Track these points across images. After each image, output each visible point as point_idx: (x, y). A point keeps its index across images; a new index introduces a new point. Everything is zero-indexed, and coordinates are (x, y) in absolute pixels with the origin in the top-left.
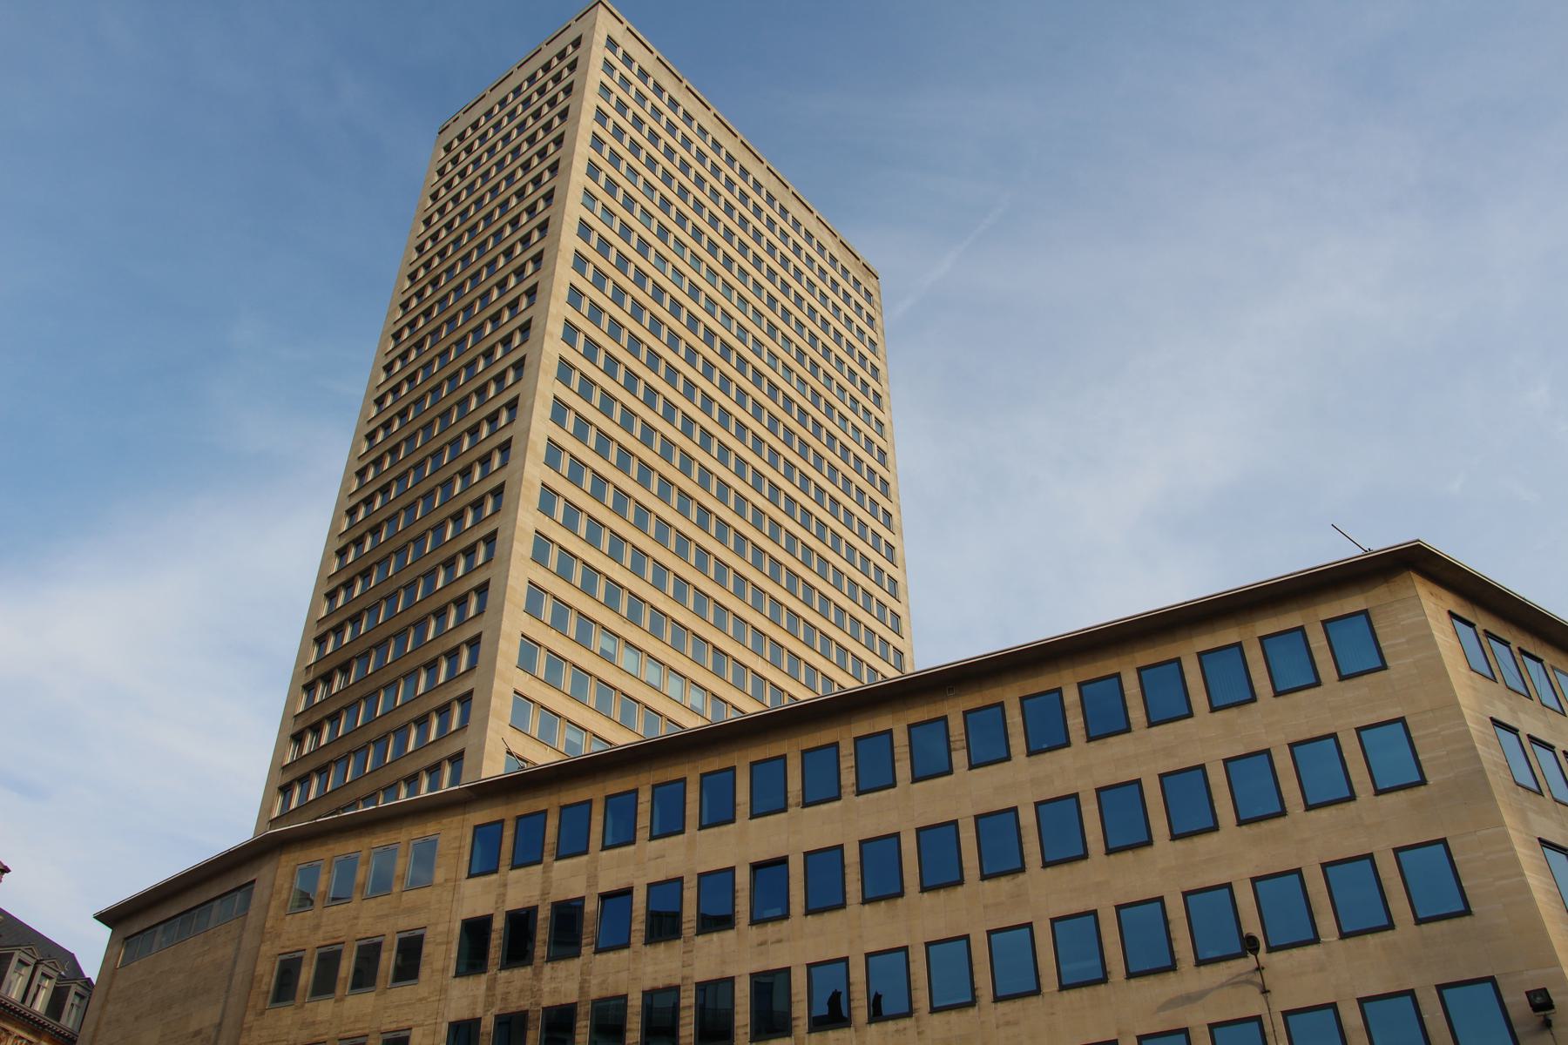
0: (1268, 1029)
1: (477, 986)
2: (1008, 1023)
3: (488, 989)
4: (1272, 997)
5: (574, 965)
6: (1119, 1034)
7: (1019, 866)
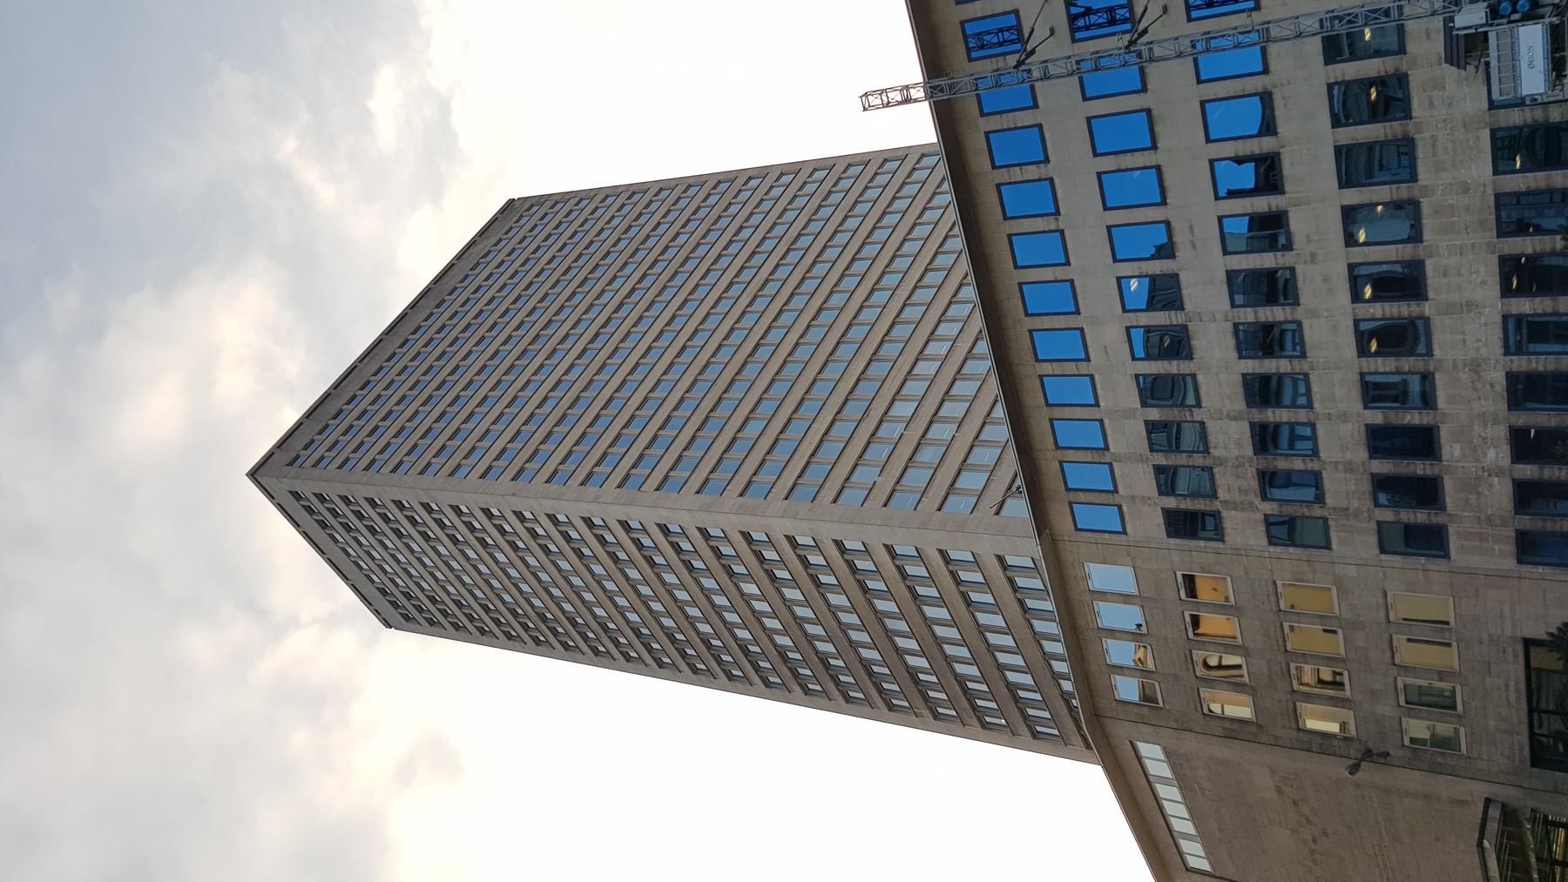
1: (1231, 519)
3: (1235, 509)
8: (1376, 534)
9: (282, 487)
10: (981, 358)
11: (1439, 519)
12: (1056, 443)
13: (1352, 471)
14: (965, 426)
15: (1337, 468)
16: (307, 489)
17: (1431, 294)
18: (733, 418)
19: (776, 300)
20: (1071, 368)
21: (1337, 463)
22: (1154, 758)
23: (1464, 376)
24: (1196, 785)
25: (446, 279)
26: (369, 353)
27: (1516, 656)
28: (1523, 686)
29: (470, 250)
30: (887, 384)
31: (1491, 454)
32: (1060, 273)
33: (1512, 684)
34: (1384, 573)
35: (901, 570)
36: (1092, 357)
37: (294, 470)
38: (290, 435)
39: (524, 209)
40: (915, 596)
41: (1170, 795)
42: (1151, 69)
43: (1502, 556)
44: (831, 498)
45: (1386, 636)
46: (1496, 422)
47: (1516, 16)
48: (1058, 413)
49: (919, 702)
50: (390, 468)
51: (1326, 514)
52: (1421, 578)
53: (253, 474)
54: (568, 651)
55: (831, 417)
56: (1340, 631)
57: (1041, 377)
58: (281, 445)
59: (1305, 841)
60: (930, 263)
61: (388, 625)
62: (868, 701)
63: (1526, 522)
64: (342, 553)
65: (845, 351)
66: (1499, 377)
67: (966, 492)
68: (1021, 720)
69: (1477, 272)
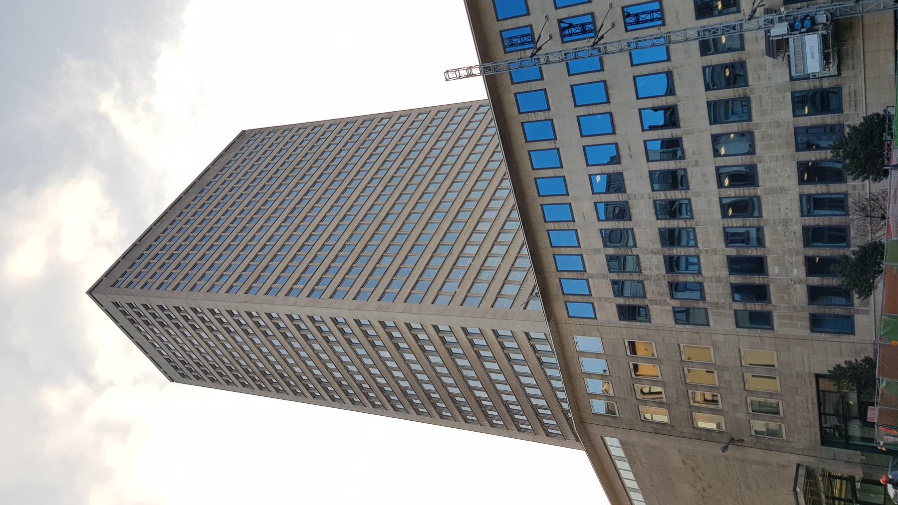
1: (654, 310)
2: (677, 17)
3: (656, 304)
8: (733, 317)
9: (108, 300)
12: (557, 268)
14: (506, 259)
16: (123, 300)
17: (761, 183)
21: (711, 277)
23: (780, 228)
25: (205, 176)
31: (795, 272)
33: (809, 399)
37: (114, 289)
39: (251, 136)
43: (802, 328)
46: (797, 254)
49: (482, 417)
51: (706, 306)
53: (90, 292)
54: (279, 393)
56: (715, 372)
57: (548, 231)
60: (485, 167)
61: (172, 380)
62: (453, 417)
63: (815, 309)
65: (438, 217)
66: (798, 229)
68: (540, 426)
69: (785, 171)
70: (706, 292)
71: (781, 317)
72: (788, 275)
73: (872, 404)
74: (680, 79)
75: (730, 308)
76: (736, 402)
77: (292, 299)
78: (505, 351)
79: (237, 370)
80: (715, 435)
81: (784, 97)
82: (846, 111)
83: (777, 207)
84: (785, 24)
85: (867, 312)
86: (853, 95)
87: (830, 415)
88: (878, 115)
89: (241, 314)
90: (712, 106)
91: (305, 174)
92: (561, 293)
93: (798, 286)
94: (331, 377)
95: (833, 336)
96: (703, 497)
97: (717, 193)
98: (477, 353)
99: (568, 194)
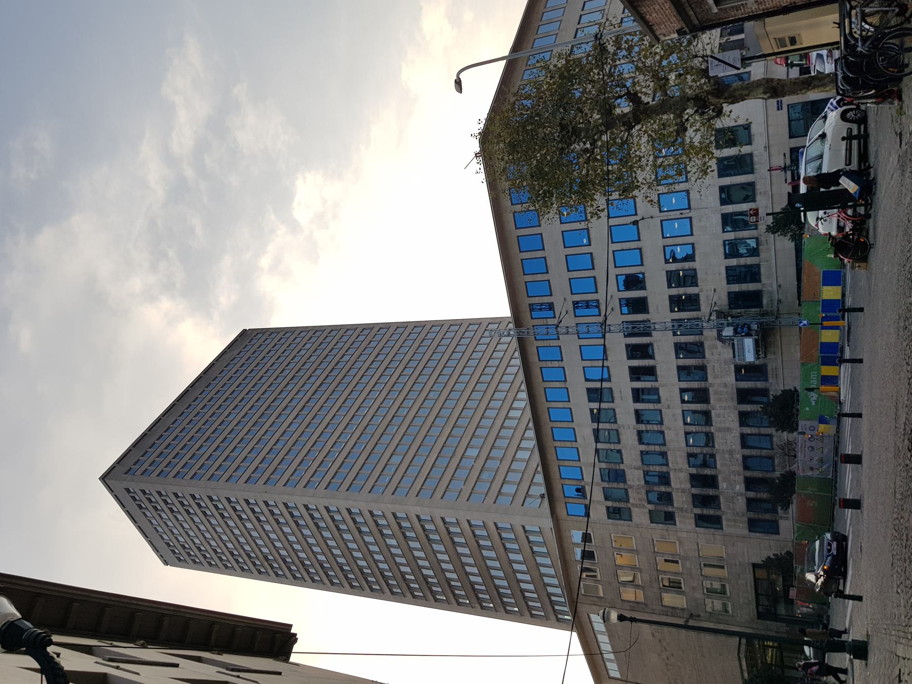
0: (666, 218)
1: (635, 512)
2: (657, 309)
3: (637, 507)
4: (654, 215)
5: (628, 472)
6: (663, 270)
7: (593, 279)
8: (694, 519)
9: (119, 486)
10: (529, 439)
11: (718, 513)
12: (561, 476)
13: (684, 492)
14: (504, 462)
15: (678, 492)
16: (135, 487)
17: (714, 424)
18: (385, 454)
19: (402, 393)
20: (568, 444)
21: (678, 489)
22: (598, 623)
23: (727, 456)
24: (616, 635)
25: (210, 372)
26: (168, 412)
27: (750, 571)
28: (753, 583)
29: (223, 356)
30: (463, 439)
31: (738, 487)
32: (566, 405)
33: (748, 583)
34: (697, 536)
35: (423, 527)
36: (578, 440)
37: (129, 476)
38: (125, 456)
39: (253, 335)
40: (405, 537)
41: (603, 639)
42: (607, 335)
43: (742, 529)
44: (440, 496)
45: (698, 563)
46: (739, 475)
47: (743, 334)
48: (562, 463)
49: (474, 600)
50: (190, 477)
51: (674, 510)
52: (712, 538)
53: (104, 478)
54: (278, 577)
55: (436, 455)
56: (680, 561)
57: (555, 447)
58: (119, 461)
59: (663, 659)
60: (478, 380)
61: (166, 563)
62: (448, 601)
63: (752, 515)
64: (148, 523)
65: (440, 422)
66: (739, 457)
67: (507, 495)
68: (526, 608)
69: (730, 416)
70: (674, 499)
71: (728, 520)
72: (732, 490)
73: (793, 586)
74: (658, 349)
75: (692, 512)
76: (695, 585)
77: (310, 491)
78: (426, 533)
79: (223, 553)
80: (678, 611)
81: (729, 368)
82: (770, 381)
83: (725, 441)
84: (732, 328)
85: (787, 519)
86: (774, 370)
87: (762, 595)
88: (790, 390)
89: (259, 503)
90: (680, 369)
91: (300, 369)
92: (563, 496)
93: (740, 498)
94: (335, 563)
95: (764, 535)
96: (667, 664)
97: (683, 428)
98: (404, 534)
99: (573, 421)
